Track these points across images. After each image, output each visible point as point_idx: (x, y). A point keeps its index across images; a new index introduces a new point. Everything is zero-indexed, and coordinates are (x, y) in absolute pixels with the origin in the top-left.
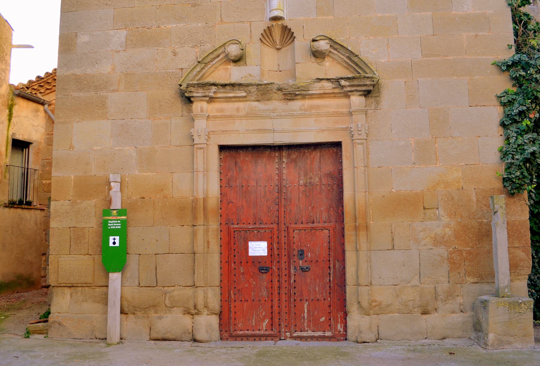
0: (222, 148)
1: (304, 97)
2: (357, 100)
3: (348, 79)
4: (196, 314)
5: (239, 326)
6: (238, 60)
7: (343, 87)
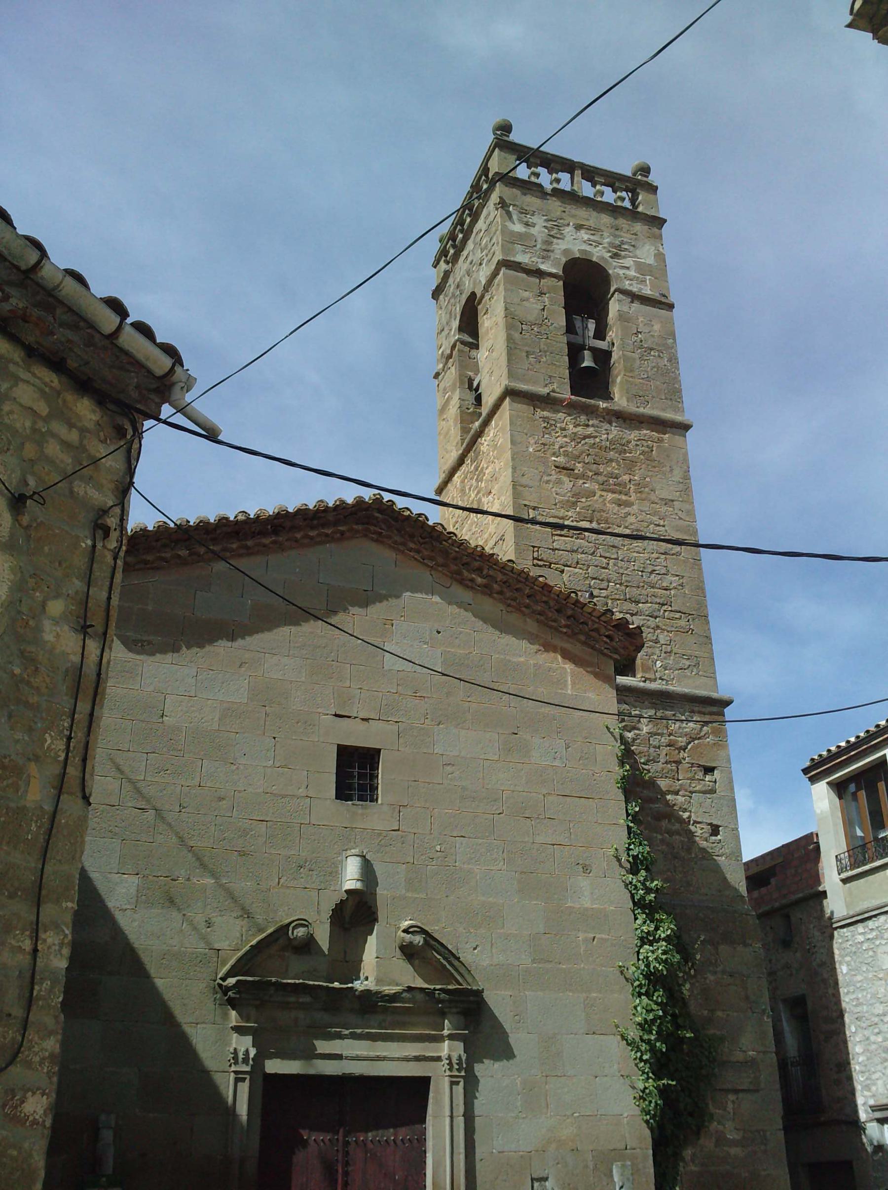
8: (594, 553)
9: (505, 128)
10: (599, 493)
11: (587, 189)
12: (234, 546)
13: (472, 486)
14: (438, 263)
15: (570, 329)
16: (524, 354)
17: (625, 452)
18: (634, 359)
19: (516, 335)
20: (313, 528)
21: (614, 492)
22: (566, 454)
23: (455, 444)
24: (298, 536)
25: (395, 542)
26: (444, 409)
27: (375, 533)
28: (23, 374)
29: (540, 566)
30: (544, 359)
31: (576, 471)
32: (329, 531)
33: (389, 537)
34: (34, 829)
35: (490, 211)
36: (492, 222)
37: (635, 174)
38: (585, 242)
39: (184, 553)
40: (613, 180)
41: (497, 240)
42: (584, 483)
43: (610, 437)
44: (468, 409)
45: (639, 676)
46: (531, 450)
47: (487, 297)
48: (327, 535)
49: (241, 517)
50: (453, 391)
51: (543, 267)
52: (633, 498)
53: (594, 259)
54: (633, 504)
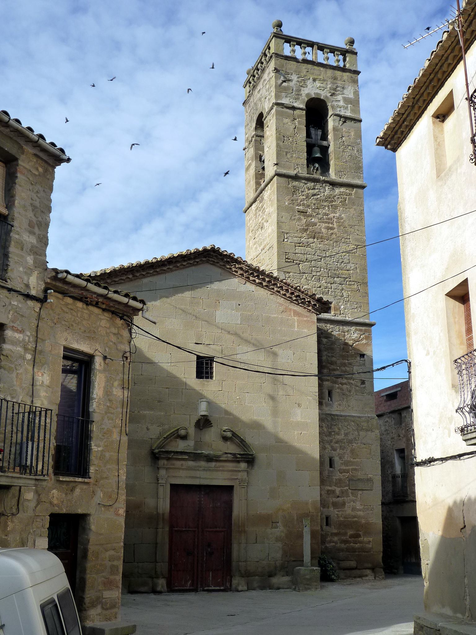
0: (172, 485)
1: (217, 461)
2: (243, 465)
3: (240, 454)
4: (155, 578)
5: (176, 584)
6: (184, 438)
7: (238, 458)
9: (279, 25)
11: (320, 57)
12: (151, 272)
15: (308, 135)
16: (285, 153)
17: (332, 201)
19: (281, 143)
20: (185, 261)
21: (326, 222)
22: (304, 205)
24: (178, 265)
25: (221, 265)
26: (248, 169)
27: (212, 261)
28: (103, 317)
30: (294, 155)
32: (192, 262)
33: (218, 263)
34: (116, 446)
39: (130, 276)
40: (333, 50)
43: (326, 194)
45: (333, 313)
48: (191, 264)
49: (154, 261)
50: (252, 161)
51: (296, 105)
52: (335, 226)
53: (322, 98)
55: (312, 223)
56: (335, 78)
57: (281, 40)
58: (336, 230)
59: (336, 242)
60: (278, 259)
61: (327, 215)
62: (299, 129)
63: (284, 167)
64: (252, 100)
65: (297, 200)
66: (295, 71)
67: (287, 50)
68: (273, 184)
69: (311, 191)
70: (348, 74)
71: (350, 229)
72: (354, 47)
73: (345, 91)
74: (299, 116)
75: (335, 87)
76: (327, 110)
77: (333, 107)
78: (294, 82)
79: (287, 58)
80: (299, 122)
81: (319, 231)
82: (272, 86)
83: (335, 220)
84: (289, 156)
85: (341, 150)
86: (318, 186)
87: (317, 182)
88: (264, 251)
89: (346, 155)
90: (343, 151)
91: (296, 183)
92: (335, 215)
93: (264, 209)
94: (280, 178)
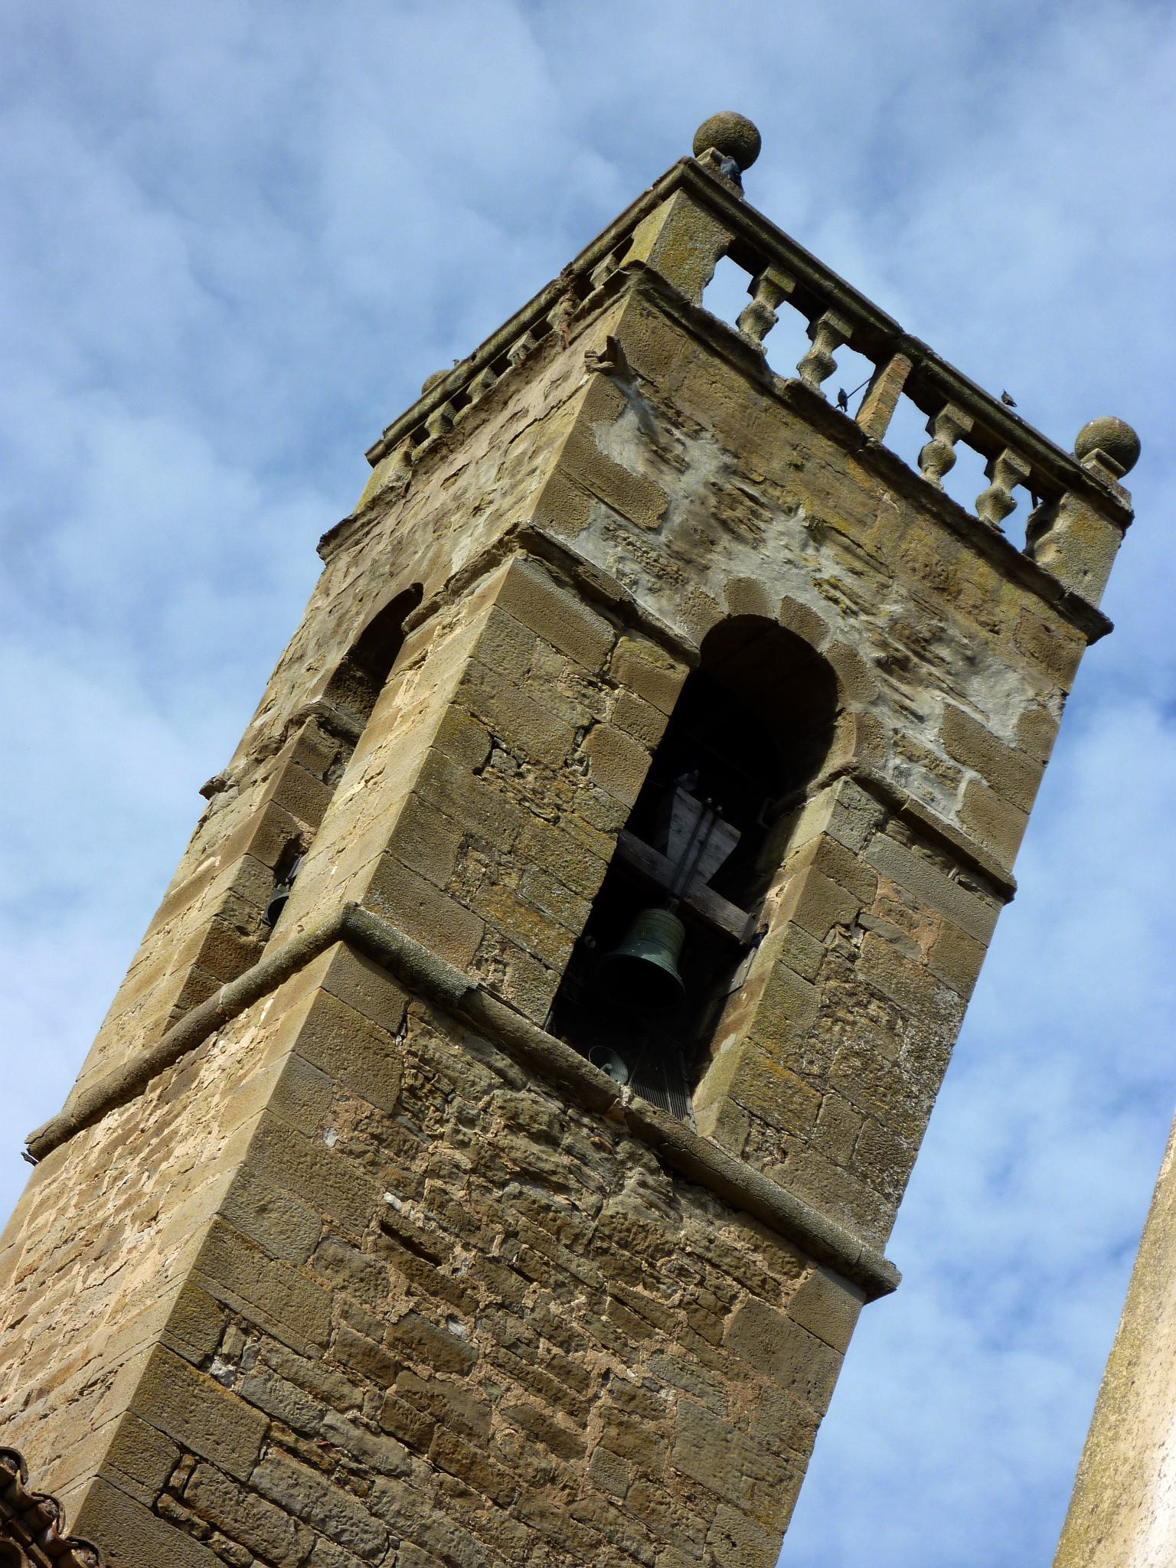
8: (373, 1553)
9: (739, 145)
10: (485, 1370)
11: (906, 432)
13: (123, 1173)
14: (385, 454)
15: (647, 818)
16: (456, 838)
17: (634, 1275)
18: (806, 1002)
19: (460, 772)
21: (537, 1386)
22: (439, 1202)
23: (149, 1021)
29: (176, 1522)
30: (511, 881)
31: (443, 1270)
35: (570, 371)
36: (561, 404)
37: (1082, 452)
38: (818, 584)
40: (994, 430)
41: (546, 460)
42: (452, 1318)
43: (612, 1206)
44: (243, 931)
46: (330, 1141)
47: (445, 614)
50: (228, 859)
51: (647, 604)
52: (589, 1436)
53: (823, 647)
54: (579, 1452)
55: (450, 1344)
56: (946, 587)
57: (715, 227)
58: (585, 1465)
59: (555, 1544)
60: (109, 1463)
61: (566, 1345)
62: (608, 748)
63: (415, 915)
64: (389, 522)
65: (412, 1152)
66: (725, 430)
67: (727, 293)
68: (299, 989)
69: (521, 1142)
70: (1030, 600)
71: (679, 1507)
72: (1123, 482)
73: (976, 684)
74: (640, 680)
75: (923, 629)
76: (825, 739)
77: (866, 731)
78: (691, 481)
79: (707, 331)
80: (623, 709)
81: (469, 1413)
82: (550, 442)
83: (605, 1399)
84: (474, 865)
85: (817, 995)
86: (582, 1135)
87: (587, 1111)
88: (38, 1407)
89: (839, 1039)
90: (827, 1011)
91: (447, 1050)
92: (619, 1368)
93: (166, 1142)
94: (358, 972)
